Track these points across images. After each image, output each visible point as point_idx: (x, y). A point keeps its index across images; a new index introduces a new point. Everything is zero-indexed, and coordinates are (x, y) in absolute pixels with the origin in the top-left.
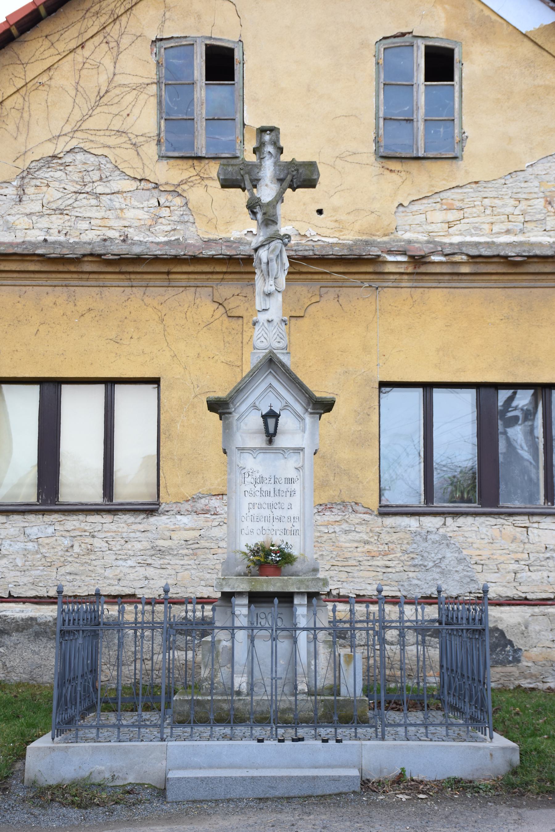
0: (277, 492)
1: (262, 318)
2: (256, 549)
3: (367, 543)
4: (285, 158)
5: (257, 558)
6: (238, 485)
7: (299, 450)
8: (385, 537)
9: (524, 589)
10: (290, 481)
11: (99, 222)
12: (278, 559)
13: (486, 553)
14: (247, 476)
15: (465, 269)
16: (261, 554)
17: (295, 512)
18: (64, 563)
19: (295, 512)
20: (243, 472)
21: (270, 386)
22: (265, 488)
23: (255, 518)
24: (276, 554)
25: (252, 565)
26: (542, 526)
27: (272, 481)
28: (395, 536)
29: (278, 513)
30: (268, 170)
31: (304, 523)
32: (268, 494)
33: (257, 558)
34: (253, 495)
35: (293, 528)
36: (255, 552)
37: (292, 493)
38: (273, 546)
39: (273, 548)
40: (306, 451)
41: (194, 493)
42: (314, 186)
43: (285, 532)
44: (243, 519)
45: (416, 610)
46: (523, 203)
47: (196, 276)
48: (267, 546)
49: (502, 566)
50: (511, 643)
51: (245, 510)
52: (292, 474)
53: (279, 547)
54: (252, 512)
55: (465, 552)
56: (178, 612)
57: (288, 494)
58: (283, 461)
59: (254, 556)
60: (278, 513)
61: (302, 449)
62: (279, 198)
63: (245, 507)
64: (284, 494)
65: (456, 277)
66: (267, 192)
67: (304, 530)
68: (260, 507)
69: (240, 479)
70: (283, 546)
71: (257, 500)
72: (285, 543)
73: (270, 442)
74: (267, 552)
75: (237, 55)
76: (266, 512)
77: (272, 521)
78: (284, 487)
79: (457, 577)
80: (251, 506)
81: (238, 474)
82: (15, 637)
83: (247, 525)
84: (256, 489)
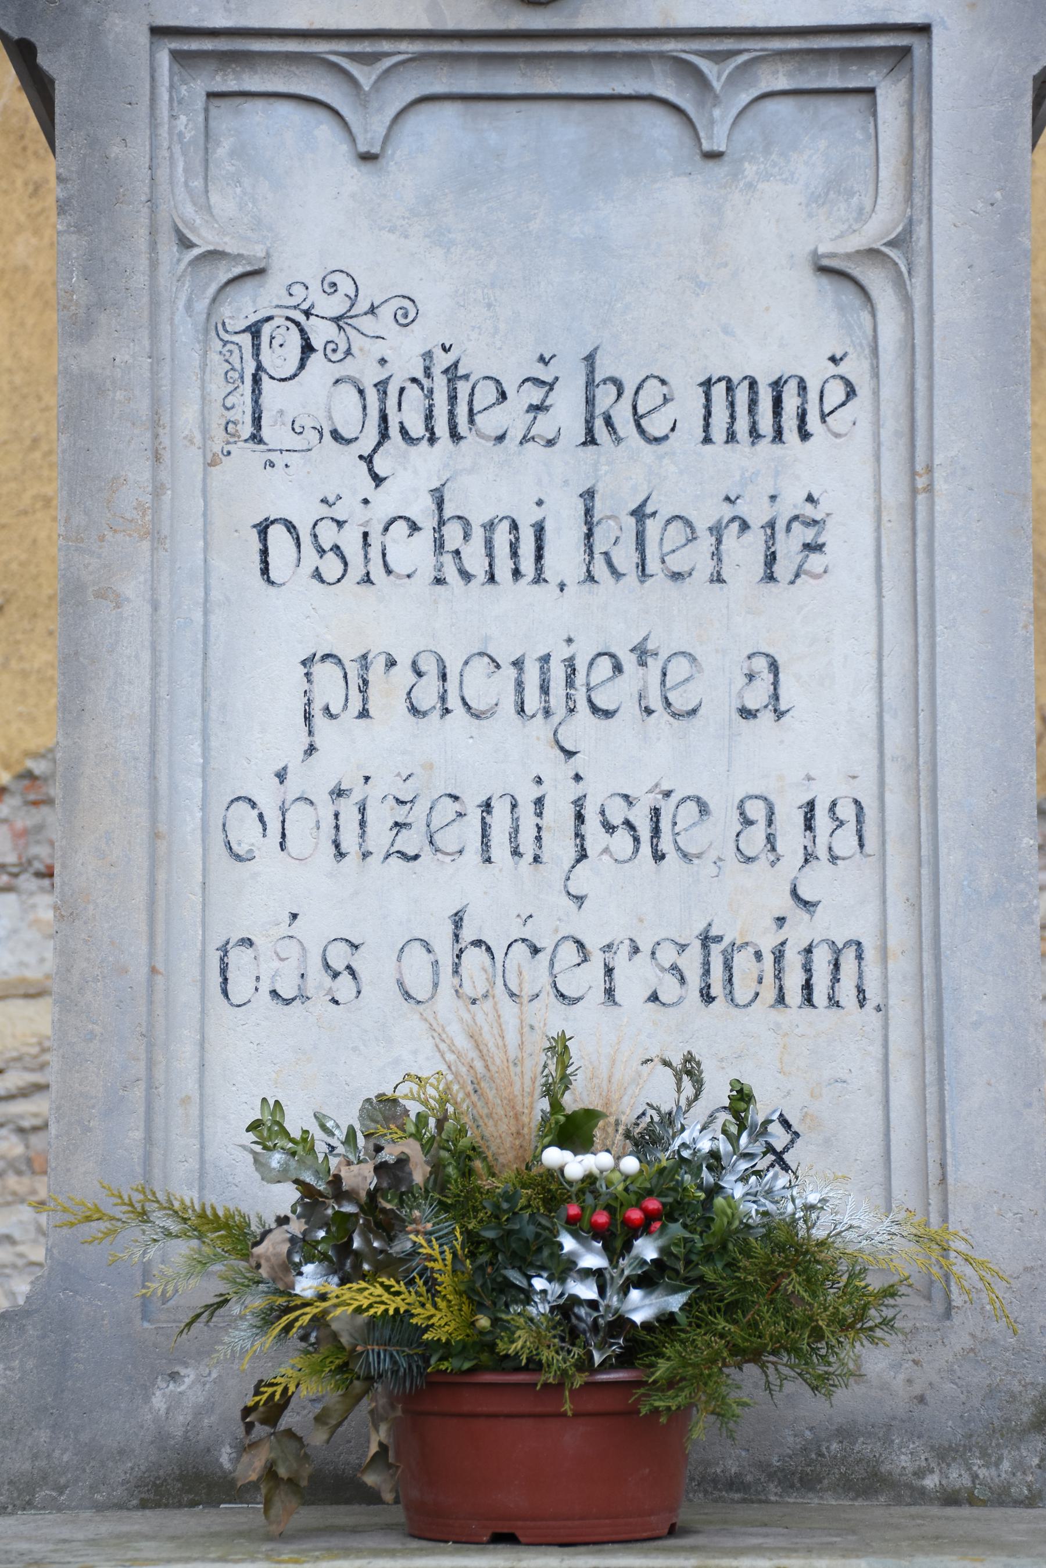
0: (615, 535)
2: (361, 1177)
5: (372, 1297)
6: (191, 461)
10: (765, 409)
12: (641, 1307)
14: (281, 357)
16: (424, 1236)
17: (824, 744)
19: (822, 748)
20: (243, 307)
22: (493, 484)
23: (380, 818)
24: (616, 1240)
25: (311, 1391)
27: (567, 411)
31: (927, 863)
32: (526, 552)
33: (372, 1297)
34: (350, 560)
35: (801, 931)
36: (350, 1223)
37: (790, 544)
38: (575, 1131)
39: (575, 1166)
40: (948, 59)
41: (35, 743)
43: (712, 966)
44: (245, 831)
45: (945, 1218)
48: (506, 1124)
51: (261, 733)
52: (788, 333)
53: (645, 1141)
54: (345, 749)
57: (744, 553)
58: (682, 195)
59: (344, 1264)
60: (626, 759)
61: (898, 46)
64: (698, 557)
67: (931, 944)
68: (437, 691)
69: (201, 393)
70: (698, 1137)
71: (395, 619)
72: (717, 1092)
74: (505, 1207)
76: (498, 756)
77: (560, 847)
78: (690, 476)
80: (328, 684)
81: (183, 329)
83: (286, 894)
84: (387, 502)
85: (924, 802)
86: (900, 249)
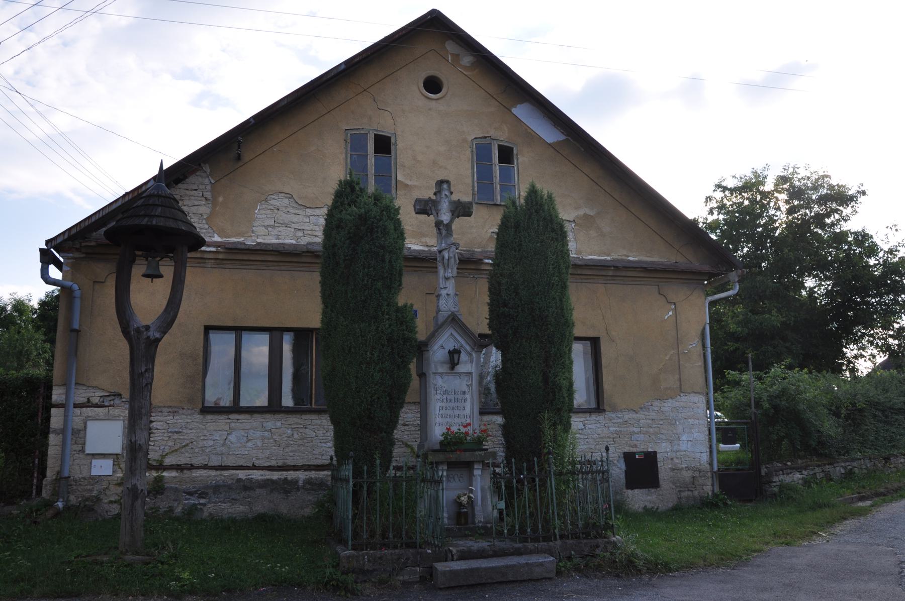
1: (444, 292)
4: (455, 197)
7: (469, 374)
10: (464, 393)
11: (309, 232)
17: (468, 411)
18: (288, 445)
21: (452, 334)
29: (457, 412)
30: (445, 206)
32: (451, 401)
42: (470, 216)
52: (465, 388)
60: (457, 412)
61: (471, 373)
62: (452, 221)
63: (438, 408)
66: (445, 217)
69: (433, 392)
73: (452, 368)
75: (393, 140)
76: (449, 412)
78: (460, 397)
82: (258, 491)
83: (439, 420)
85: (245, 257)
86: (471, 385)
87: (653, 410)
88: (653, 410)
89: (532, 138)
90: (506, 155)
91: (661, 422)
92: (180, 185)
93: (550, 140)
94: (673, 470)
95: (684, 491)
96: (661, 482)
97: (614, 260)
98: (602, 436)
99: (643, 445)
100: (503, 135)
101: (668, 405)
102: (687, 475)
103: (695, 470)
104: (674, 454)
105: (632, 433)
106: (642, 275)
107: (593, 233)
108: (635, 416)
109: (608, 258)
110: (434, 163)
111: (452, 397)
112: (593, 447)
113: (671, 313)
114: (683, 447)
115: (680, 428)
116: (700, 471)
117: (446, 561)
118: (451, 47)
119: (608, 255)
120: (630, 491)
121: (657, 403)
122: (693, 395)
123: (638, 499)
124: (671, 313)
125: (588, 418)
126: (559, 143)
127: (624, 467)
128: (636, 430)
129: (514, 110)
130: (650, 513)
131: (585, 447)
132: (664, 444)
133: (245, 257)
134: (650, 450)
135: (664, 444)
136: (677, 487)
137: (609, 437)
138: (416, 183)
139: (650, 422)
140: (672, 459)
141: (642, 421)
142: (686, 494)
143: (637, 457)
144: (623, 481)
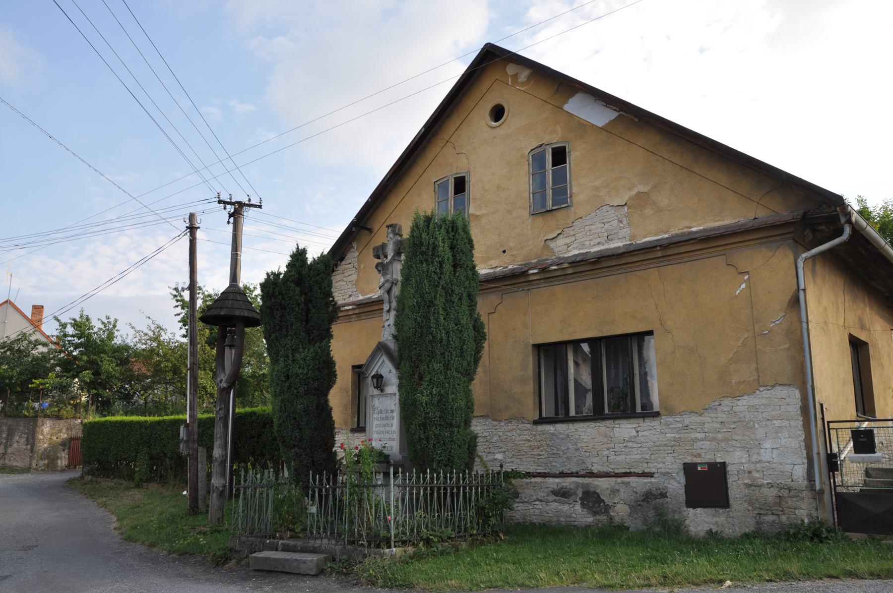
3: (529, 441)
8: (538, 438)
9: (612, 467)
10: (392, 411)
13: (591, 446)
15: (570, 271)
26: (622, 426)
28: (543, 436)
29: (387, 429)
46: (607, 225)
47: (716, 249)
49: (600, 453)
50: (603, 501)
55: (579, 445)
56: (243, 474)
60: (387, 429)
65: (666, 259)
76: (382, 429)
79: (575, 460)
87: (723, 411)
88: (723, 411)
89: (583, 127)
90: (560, 156)
91: (734, 426)
92: (343, 262)
93: (600, 124)
94: (748, 486)
95: (766, 514)
96: (731, 501)
97: (672, 237)
98: (658, 444)
99: (706, 453)
100: (554, 137)
101: (743, 404)
102: (770, 494)
103: (781, 487)
104: (752, 467)
105: (696, 440)
106: (698, 247)
107: (649, 211)
108: (699, 419)
109: (667, 236)
110: (499, 187)
111: (383, 416)
112: (647, 457)
113: (743, 286)
114: (766, 456)
115: (760, 433)
116: (790, 490)
117: (277, 550)
118: (511, 69)
119: (665, 233)
120: (691, 510)
121: (727, 402)
122: (778, 388)
123: (700, 521)
124: (743, 286)
125: (642, 424)
126: (612, 123)
127: (683, 480)
128: (699, 436)
129: (566, 107)
130: (711, 542)
131: (638, 457)
132: (738, 453)
133: (369, 309)
134: (718, 460)
135: (738, 453)
136: (755, 509)
137: (666, 445)
138: (484, 212)
139: (718, 426)
140: (750, 472)
141: (707, 425)
142: (770, 518)
143: (699, 469)
144: (682, 497)
